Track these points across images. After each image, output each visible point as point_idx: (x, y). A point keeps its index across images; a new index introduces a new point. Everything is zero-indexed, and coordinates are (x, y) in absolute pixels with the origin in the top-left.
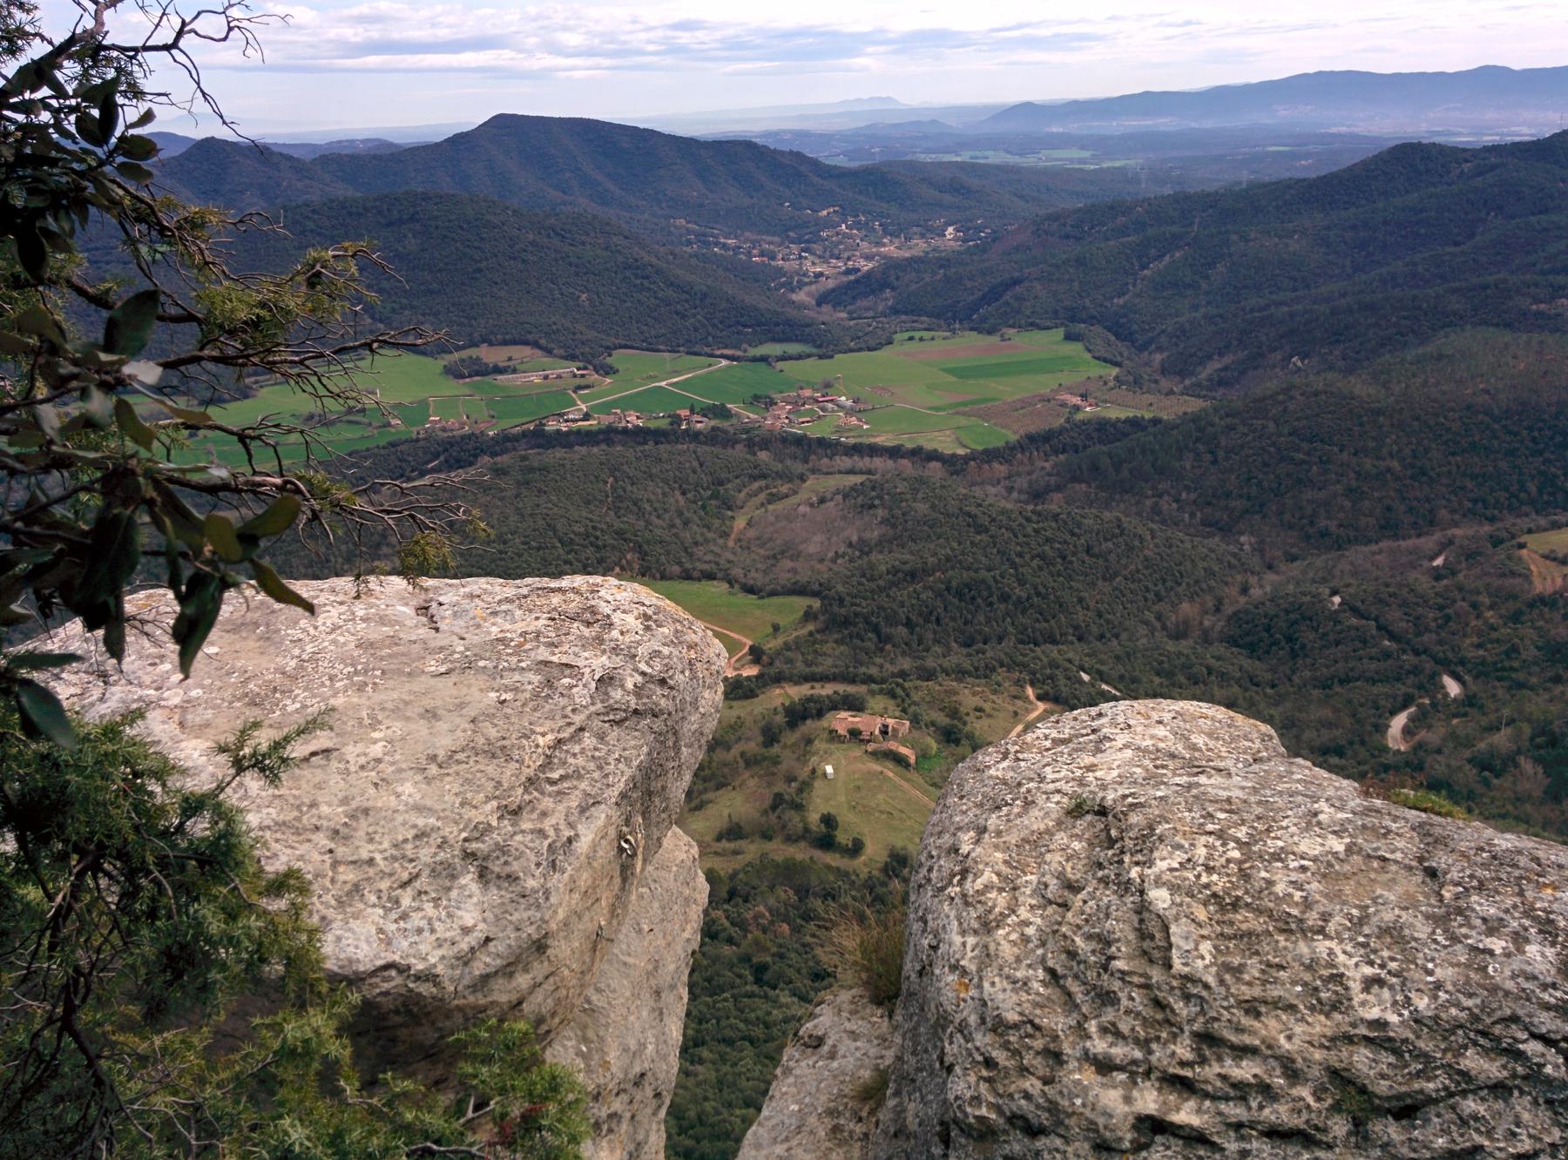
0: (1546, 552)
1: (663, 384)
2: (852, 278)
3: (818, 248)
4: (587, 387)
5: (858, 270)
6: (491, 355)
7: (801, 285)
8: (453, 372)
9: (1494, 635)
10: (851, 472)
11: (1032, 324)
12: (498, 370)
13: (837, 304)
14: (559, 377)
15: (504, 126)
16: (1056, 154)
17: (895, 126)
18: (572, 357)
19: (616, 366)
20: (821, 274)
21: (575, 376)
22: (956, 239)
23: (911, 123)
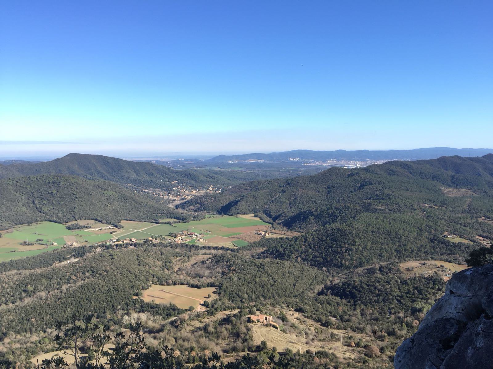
0: (407, 268)
1: (140, 231)
2: (184, 201)
3: (173, 193)
4: (114, 232)
5: (186, 199)
6: (82, 223)
7: (169, 203)
8: (69, 228)
9: (130, 295)
10: (205, 254)
11: (244, 213)
12: (84, 227)
13: (183, 208)
14: (105, 229)
15: (73, 157)
16: (233, 169)
17: (463, 150)
18: (108, 223)
19: (123, 225)
20: (175, 200)
21: (110, 229)
22: (213, 190)
23: (487, 149)
